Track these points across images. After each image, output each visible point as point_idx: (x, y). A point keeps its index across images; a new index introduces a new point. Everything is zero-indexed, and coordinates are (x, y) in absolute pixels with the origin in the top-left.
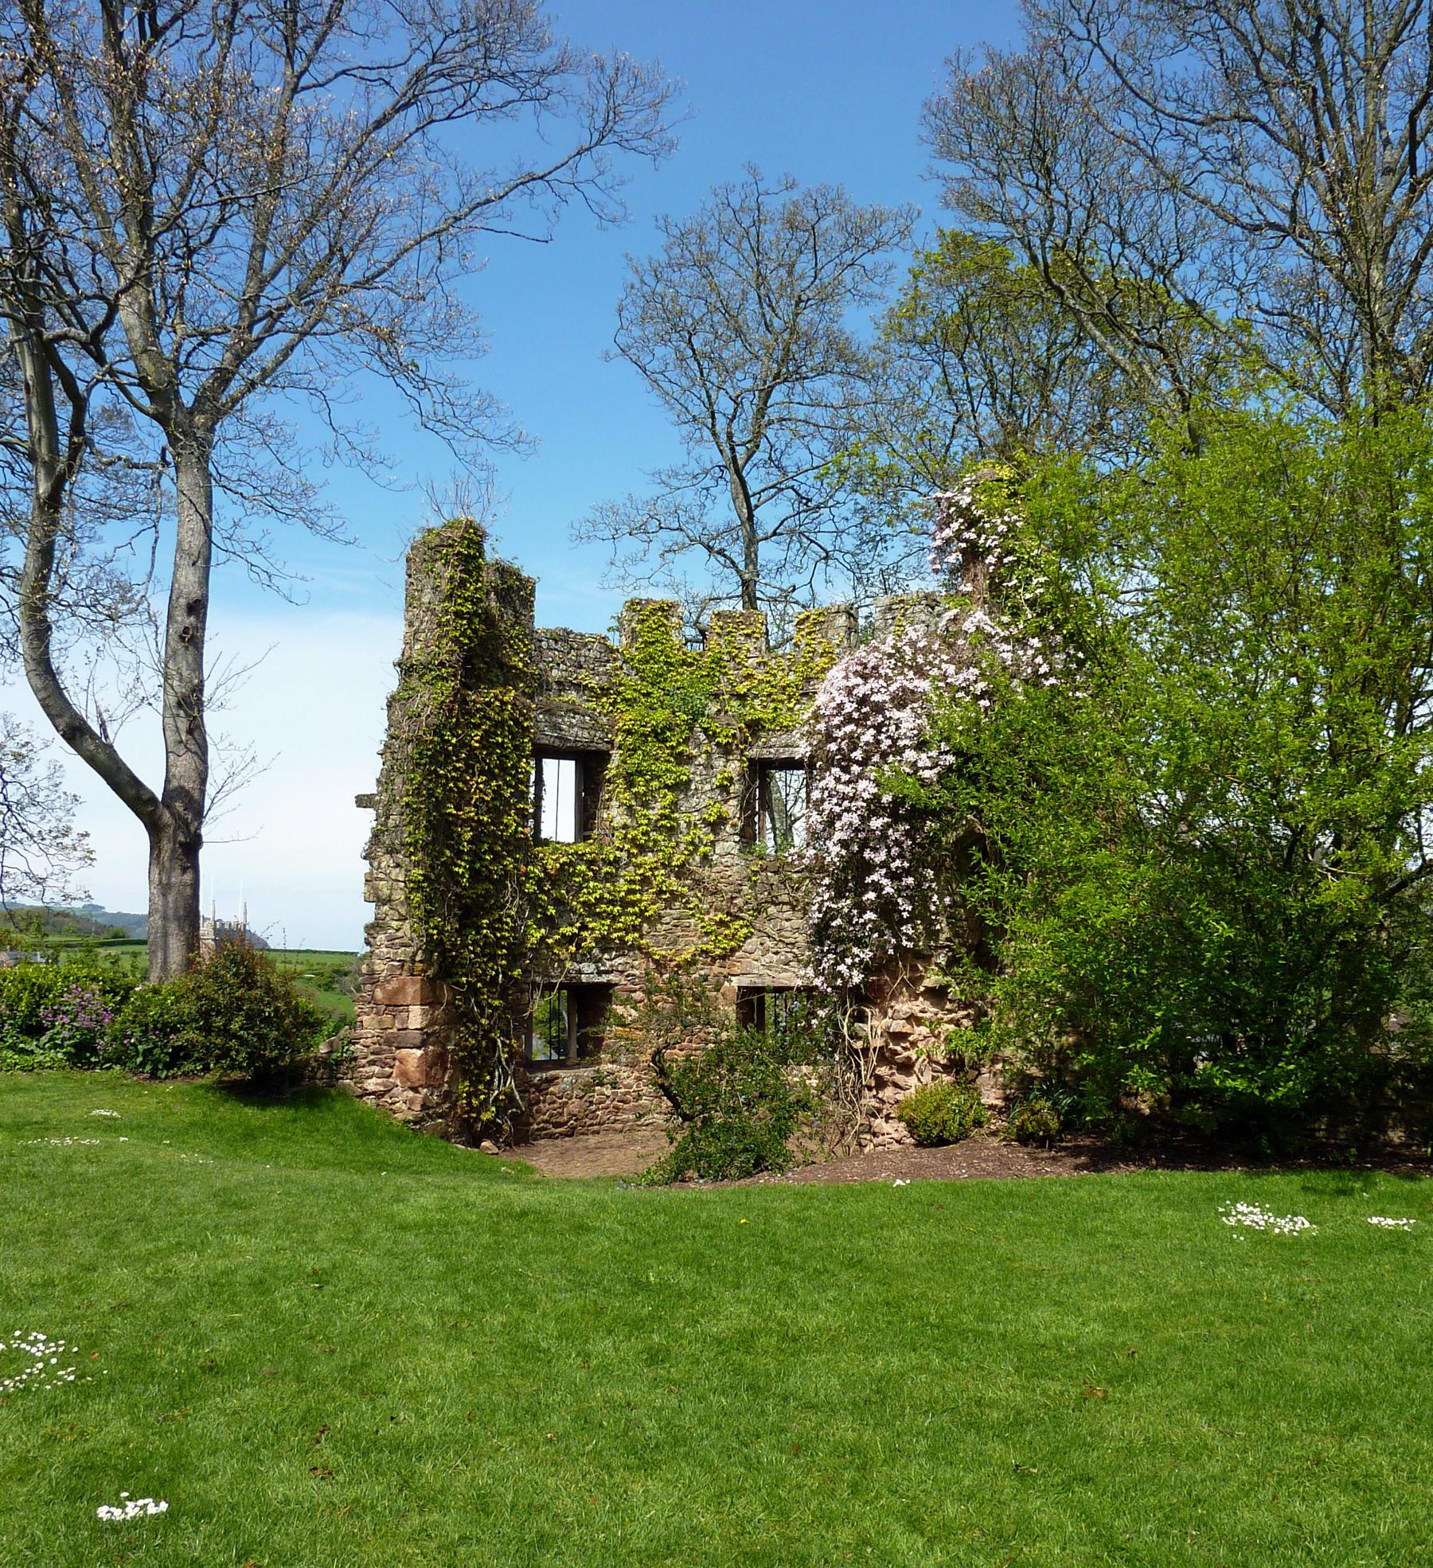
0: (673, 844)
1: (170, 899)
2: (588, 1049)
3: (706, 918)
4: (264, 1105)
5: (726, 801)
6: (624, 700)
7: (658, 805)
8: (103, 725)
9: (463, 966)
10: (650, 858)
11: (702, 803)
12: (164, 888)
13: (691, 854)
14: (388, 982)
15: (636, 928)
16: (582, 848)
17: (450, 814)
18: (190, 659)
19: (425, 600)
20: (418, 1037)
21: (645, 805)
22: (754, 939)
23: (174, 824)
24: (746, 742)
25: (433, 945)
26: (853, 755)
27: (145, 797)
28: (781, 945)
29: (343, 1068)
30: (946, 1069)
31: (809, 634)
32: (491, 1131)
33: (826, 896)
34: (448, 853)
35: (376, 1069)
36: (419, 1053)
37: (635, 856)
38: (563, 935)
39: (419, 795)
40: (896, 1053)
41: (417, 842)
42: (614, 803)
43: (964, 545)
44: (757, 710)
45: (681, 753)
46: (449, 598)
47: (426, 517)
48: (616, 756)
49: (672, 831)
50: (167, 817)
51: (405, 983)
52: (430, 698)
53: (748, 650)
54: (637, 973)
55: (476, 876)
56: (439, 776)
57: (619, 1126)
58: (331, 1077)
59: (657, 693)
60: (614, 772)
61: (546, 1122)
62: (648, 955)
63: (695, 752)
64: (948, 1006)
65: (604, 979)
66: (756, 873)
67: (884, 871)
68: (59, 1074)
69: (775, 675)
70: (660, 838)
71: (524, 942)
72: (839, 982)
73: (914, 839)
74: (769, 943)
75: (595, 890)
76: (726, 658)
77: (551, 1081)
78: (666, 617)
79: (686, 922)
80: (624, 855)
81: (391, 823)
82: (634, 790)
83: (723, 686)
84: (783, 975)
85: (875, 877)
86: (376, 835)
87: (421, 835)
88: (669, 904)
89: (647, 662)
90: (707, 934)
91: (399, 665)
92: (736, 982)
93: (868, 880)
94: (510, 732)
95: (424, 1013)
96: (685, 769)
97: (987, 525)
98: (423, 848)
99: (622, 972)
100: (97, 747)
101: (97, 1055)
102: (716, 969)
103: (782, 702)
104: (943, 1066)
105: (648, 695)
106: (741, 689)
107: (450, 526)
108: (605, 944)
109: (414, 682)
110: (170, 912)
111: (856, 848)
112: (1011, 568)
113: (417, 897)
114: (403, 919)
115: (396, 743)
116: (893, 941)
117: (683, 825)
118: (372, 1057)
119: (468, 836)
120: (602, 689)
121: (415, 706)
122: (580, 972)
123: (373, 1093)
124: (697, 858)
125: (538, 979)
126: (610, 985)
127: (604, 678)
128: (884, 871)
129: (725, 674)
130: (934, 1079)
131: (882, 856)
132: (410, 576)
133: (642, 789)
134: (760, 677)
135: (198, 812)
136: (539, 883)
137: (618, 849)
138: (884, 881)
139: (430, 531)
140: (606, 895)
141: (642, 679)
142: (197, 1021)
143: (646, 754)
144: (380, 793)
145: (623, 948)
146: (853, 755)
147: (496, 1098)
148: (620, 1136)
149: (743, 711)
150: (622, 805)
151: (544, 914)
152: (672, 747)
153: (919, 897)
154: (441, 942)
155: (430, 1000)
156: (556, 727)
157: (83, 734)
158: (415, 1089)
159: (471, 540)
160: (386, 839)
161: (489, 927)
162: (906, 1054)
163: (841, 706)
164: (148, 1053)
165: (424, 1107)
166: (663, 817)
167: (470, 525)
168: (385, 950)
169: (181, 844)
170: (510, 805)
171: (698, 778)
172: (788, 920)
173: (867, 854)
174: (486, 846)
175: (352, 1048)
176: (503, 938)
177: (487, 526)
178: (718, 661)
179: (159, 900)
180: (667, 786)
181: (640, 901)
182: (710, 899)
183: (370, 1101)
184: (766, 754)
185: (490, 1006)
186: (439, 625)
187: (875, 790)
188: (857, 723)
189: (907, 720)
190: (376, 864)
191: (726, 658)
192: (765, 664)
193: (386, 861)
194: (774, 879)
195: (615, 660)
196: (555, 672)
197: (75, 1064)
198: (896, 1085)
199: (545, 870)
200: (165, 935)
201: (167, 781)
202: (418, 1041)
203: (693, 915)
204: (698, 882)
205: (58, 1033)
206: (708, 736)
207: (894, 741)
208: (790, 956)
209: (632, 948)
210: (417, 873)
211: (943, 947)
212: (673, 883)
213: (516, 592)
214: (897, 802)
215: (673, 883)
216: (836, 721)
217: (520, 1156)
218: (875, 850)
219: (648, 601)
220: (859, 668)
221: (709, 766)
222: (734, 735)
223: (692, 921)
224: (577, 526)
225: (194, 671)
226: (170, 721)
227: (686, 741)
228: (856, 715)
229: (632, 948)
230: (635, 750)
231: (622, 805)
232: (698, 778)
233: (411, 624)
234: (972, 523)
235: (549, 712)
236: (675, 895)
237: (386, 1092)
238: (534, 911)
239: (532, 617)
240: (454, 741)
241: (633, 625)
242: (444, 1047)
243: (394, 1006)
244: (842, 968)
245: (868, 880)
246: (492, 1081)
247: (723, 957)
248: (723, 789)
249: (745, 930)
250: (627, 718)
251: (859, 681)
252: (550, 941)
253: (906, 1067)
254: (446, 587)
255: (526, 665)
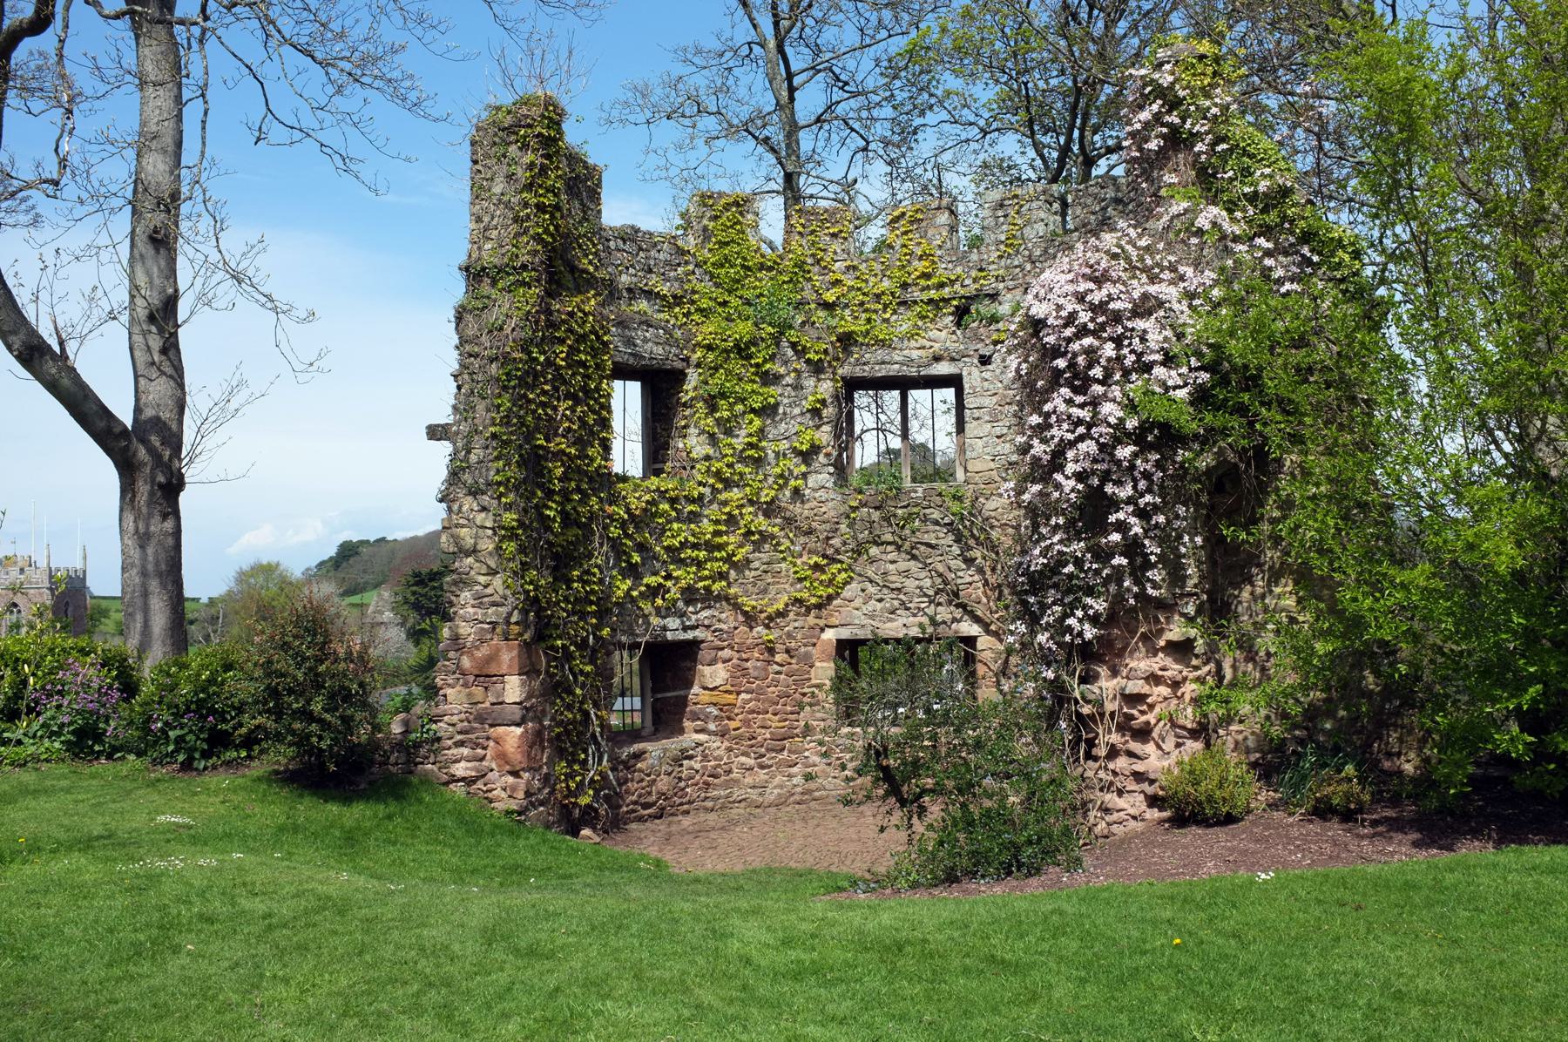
0: (761, 477)
1: (150, 551)
2: (667, 715)
3: (799, 562)
4: (347, 800)
5: (818, 427)
6: (700, 310)
7: (743, 433)
8: (61, 343)
9: (557, 627)
10: (735, 494)
11: (792, 429)
12: (143, 539)
13: (781, 488)
14: (477, 648)
15: (722, 576)
16: (654, 482)
17: (541, 447)
18: (163, 263)
19: (497, 189)
20: (517, 713)
21: (729, 432)
22: (854, 585)
23: (148, 460)
24: (838, 359)
25: (532, 603)
26: (1091, 373)
27: (117, 430)
28: (885, 591)
29: (422, 751)
30: (1194, 734)
31: (906, 233)
32: (589, 817)
33: (1056, 539)
34: (539, 493)
35: (465, 751)
36: (519, 731)
37: (719, 492)
38: (647, 586)
39: (508, 424)
40: (1133, 718)
41: (508, 480)
42: (693, 431)
43: (1165, 130)
44: (848, 322)
45: (767, 372)
46: (529, 187)
47: (483, 91)
48: (693, 378)
49: (758, 462)
50: (142, 453)
51: (498, 650)
52: (511, 308)
53: (835, 253)
54: (724, 627)
55: (567, 520)
56: (529, 401)
57: (709, 804)
58: (408, 762)
59: (734, 301)
60: (691, 394)
61: (635, 803)
62: (737, 607)
63: (782, 370)
64: (1195, 662)
65: (690, 635)
66: (854, 509)
67: (1131, 509)
68: (63, 769)
69: (866, 281)
70: (747, 470)
71: (609, 597)
72: (1068, 638)
73: (1164, 471)
74: (871, 589)
75: (679, 533)
76: (810, 261)
77: (638, 756)
78: (741, 213)
79: (776, 567)
80: (707, 491)
81: (473, 458)
82: (717, 415)
83: (808, 294)
84: (889, 625)
85: (1121, 515)
86: (454, 475)
87: (514, 473)
88: (757, 546)
89: (722, 266)
90: (800, 580)
91: (467, 269)
92: (830, 635)
93: (1112, 519)
94: (592, 348)
95: (523, 684)
96: (772, 390)
97: (1192, 108)
98: (516, 488)
99: (708, 627)
100: (60, 370)
101: (102, 743)
102: (811, 620)
103: (876, 311)
104: (1189, 731)
105: (725, 304)
106: (830, 297)
107: (525, 102)
108: (690, 595)
109: (485, 288)
110: (150, 567)
111: (1096, 482)
112: (1224, 157)
113: (510, 547)
114: (492, 572)
115: (476, 363)
116: (1136, 589)
117: (771, 455)
118: (459, 737)
119: (559, 471)
120: (674, 297)
121: (493, 316)
122: (665, 629)
123: (463, 779)
124: (788, 493)
125: (624, 639)
126: (695, 644)
127: (676, 284)
128: (1131, 509)
129: (810, 279)
130: (1178, 745)
131: (1126, 492)
132: (475, 162)
133: (726, 414)
134: (850, 283)
135: (174, 441)
136: (623, 525)
137: (700, 483)
138: (1133, 520)
139: (498, 109)
140: (691, 539)
141: (717, 285)
142: (265, 703)
143: (729, 372)
144: (458, 423)
145: (709, 598)
146: (1091, 373)
147: (592, 780)
148: (712, 816)
149: (833, 323)
150: (702, 432)
151: (628, 562)
152: (757, 365)
153: (1167, 539)
154: (536, 600)
155: (528, 670)
156: (629, 342)
157: (42, 355)
158: (515, 774)
159: (550, 118)
160: (467, 477)
161: (580, 579)
162: (1143, 719)
163: (1072, 317)
164: (180, 740)
165: (528, 794)
166: (751, 445)
167: (549, 102)
168: (471, 610)
169: (161, 486)
170: (592, 433)
171: (786, 401)
172: (893, 562)
173: (1109, 489)
174: (573, 484)
175: (434, 726)
176: (593, 592)
177: (564, 101)
178: (800, 265)
179: (136, 554)
180: (753, 411)
181: (727, 544)
182: (802, 539)
183: (459, 789)
184: (859, 372)
185: (582, 672)
186: (516, 220)
187: (1121, 414)
188: (1094, 333)
189: (1154, 332)
190: (455, 507)
191: (810, 261)
192: (855, 268)
193: (468, 503)
194: (876, 515)
195: (687, 263)
196: (624, 278)
197: (76, 755)
198: (1131, 754)
199: (628, 511)
200: (145, 594)
201: (138, 410)
202: (517, 717)
203: (784, 559)
204: (789, 521)
205: (53, 718)
206: (796, 352)
207: (1140, 355)
208: (896, 603)
209: (718, 598)
210: (510, 518)
211: (1190, 595)
212: (761, 523)
213: (583, 184)
214: (1144, 428)
215: (761, 523)
216: (1069, 332)
217: (617, 847)
218: (1119, 483)
219: (721, 195)
220: (1088, 271)
221: (797, 387)
222: (826, 352)
223: (783, 565)
224: (606, 107)
225: (167, 278)
226: (138, 339)
227: (772, 357)
228: (1091, 326)
229: (718, 598)
230: (716, 369)
231: (702, 432)
232: (786, 401)
233: (479, 220)
234: (1174, 104)
235: (621, 324)
236: (765, 537)
237: (477, 779)
238: (618, 559)
239: (599, 212)
240: (542, 358)
241: (705, 222)
242: (541, 723)
243: (486, 676)
244: (1071, 621)
245: (1112, 519)
246: (585, 761)
247: (819, 607)
248: (815, 412)
249: (844, 575)
250: (707, 330)
251: (1091, 285)
252: (635, 593)
253: (1143, 734)
254: (523, 175)
255: (596, 268)
